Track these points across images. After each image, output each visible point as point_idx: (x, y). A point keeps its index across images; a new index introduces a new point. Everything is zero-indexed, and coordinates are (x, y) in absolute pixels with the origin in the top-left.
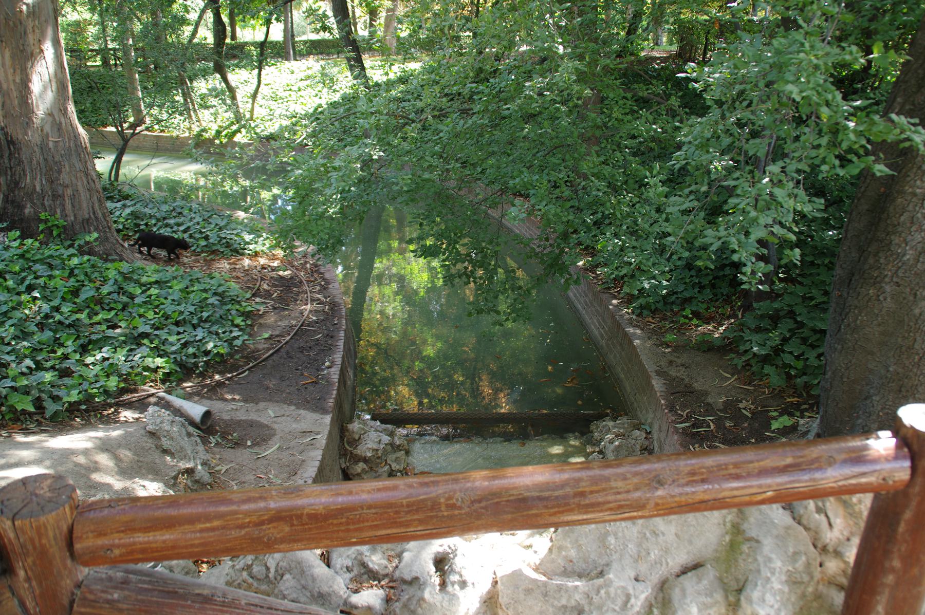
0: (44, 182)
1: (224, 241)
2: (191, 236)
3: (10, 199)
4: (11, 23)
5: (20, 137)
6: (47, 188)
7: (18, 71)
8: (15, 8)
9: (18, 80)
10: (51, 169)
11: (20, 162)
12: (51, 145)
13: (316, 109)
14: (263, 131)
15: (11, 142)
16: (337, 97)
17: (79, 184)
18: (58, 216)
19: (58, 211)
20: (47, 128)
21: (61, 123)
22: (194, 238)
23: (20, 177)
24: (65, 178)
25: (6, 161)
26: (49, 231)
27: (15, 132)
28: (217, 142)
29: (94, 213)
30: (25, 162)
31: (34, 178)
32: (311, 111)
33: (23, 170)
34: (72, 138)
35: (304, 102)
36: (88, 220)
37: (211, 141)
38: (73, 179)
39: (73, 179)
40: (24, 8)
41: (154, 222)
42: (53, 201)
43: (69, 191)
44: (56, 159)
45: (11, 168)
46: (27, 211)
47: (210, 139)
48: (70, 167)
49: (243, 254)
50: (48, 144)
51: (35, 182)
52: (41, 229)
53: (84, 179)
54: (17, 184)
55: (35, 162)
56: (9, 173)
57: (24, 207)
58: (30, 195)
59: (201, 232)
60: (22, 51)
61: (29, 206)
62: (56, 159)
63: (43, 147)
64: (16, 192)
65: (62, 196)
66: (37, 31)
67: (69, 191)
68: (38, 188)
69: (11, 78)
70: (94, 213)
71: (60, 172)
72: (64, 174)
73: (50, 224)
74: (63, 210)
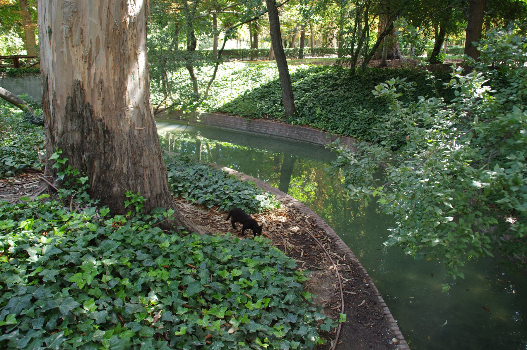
0: (130, 165)
1: (245, 201)
2: (217, 197)
3: (102, 179)
4: (117, 32)
5: (114, 127)
6: (131, 170)
7: (118, 72)
8: (121, 20)
9: (116, 80)
10: (135, 153)
11: (113, 148)
12: (136, 133)
13: (246, 93)
14: (214, 106)
15: (106, 131)
16: (258, 86)
17: (155, 165)
18: (139, 194)
19: (139, 189)
20: (135, 119)
21: (144, 114)
22: (221, 198)
23: (111, 161)
24: (145, 160)
25: (102, 148)
26: (133, 207)
27: (112, 125)
28: (184, 112)
29: (164, 189)
30: (117, 148)
31: (122, 162)
32: (243, 94)
33: (115, 155)
34: (151, 127)
35: (237, 88)
36: (160, 195)
37: (180, 112)
38: (151, 161)
39: (151, 161)
40: (128, 19)
41: (188, 184)
42: (135, 180)
43: (148, 172)
44: (139, 145)
45: (105, 153)
46: (115, 189)
47: (178, 110)
48: (149, 151)
49: (257, 212)
50: (134, 132)
51: (122, 164)
52: (126, 206)
53: (158, 160)
54: (108, 166)
55: (124, 148)
56: (103, 157)
57: (113, 186)
58: (118, 176)
59: (225, 194)
60: (122, 55)
61: (116, 185)
62: (139, 145)
63: (131, 135)
64: (107, 174)
65: (142, 176)
66: (134, 38)
67: (148, 172)
68: (125, 170)
69: (111, 77)
70: (164, 189)
71: (141, 155)
72: (144, 156)
73: (133, 201)
74: (143, 188)
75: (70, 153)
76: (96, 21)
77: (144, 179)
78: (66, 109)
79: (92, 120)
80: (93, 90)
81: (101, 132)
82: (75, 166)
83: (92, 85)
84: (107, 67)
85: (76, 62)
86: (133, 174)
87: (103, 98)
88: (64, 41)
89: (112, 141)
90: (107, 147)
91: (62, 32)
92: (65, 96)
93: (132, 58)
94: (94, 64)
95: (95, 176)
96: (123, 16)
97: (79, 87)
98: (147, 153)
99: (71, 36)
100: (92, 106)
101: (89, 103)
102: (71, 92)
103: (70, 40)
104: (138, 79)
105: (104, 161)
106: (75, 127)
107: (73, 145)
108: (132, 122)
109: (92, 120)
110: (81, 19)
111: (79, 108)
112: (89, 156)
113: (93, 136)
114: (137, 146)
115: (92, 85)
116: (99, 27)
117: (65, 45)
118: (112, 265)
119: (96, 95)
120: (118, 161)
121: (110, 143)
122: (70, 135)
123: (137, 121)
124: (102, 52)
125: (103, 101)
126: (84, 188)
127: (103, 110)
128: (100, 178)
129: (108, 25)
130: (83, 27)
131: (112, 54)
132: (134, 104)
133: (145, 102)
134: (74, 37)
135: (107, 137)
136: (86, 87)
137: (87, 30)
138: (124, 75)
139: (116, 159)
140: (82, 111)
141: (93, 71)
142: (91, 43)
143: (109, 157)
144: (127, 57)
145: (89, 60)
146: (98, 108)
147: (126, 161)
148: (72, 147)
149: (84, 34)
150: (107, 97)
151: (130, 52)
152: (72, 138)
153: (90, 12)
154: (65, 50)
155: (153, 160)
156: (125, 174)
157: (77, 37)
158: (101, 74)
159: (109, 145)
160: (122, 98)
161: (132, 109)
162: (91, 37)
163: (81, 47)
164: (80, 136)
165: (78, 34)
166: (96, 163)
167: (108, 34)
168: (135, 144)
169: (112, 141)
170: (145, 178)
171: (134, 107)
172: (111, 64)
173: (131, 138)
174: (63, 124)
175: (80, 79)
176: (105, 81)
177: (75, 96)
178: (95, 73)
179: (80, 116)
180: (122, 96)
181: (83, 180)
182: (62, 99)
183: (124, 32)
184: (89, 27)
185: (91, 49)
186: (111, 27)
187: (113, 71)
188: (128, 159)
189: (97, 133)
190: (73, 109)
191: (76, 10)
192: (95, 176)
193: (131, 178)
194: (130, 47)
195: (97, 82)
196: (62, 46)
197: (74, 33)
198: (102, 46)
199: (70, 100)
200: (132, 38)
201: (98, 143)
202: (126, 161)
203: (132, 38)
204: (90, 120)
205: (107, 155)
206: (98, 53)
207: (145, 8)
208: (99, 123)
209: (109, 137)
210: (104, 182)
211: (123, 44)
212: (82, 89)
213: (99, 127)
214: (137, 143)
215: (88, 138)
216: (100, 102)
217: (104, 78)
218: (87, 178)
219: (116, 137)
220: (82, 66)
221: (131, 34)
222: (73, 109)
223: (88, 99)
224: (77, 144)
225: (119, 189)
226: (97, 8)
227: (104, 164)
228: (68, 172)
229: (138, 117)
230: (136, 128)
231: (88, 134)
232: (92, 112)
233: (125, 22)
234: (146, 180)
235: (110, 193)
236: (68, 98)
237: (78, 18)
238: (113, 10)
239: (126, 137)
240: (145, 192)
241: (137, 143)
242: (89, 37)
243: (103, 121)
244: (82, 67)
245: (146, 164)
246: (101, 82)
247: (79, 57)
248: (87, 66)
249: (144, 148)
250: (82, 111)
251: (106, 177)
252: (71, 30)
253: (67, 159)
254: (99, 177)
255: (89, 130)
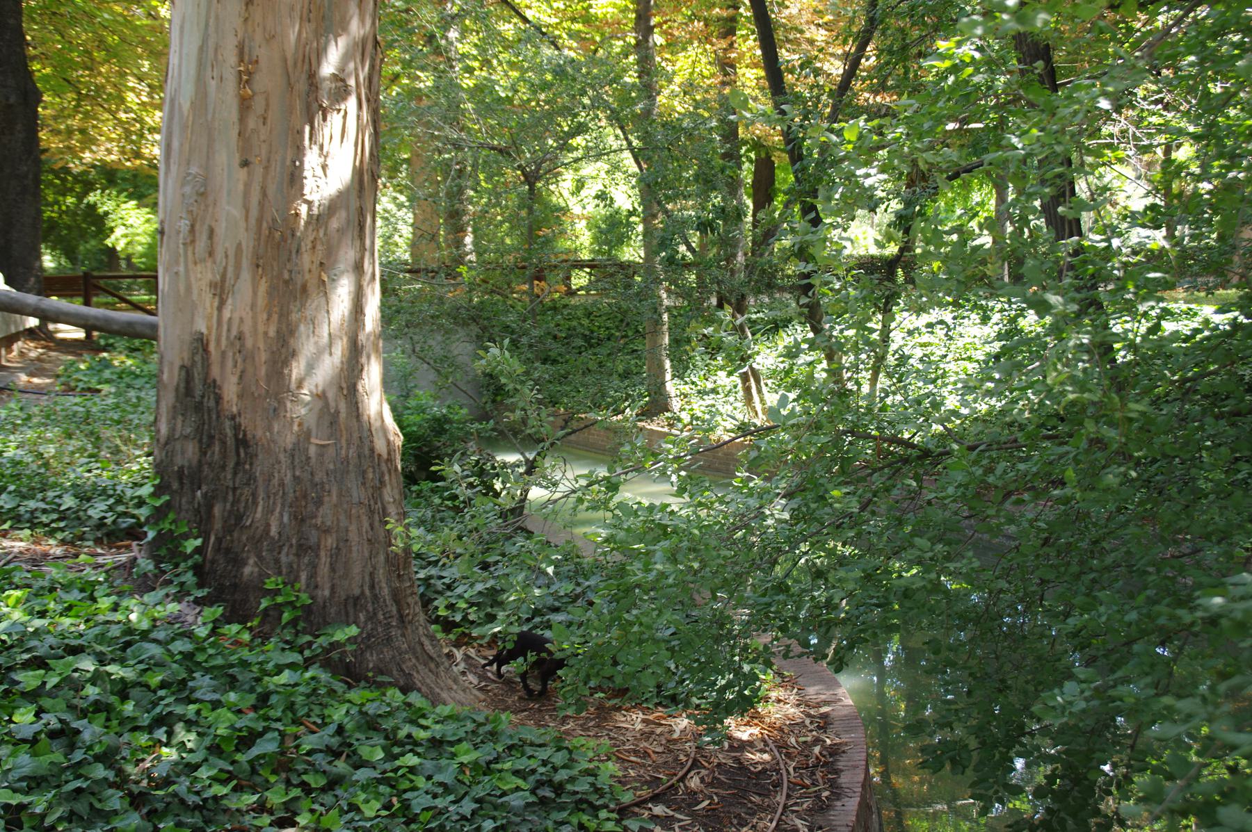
3: (224, 545)
5: (259, 433)
9: (272, 333)
11: (251, 479)
12: (312, 451)
15: (242, 442)
17: (353, 528)
19: (303, 576)
20: (312, 422)
21: (337, 412)
25: (229, 476)
27: (255, 427)
31: (269, 511)
38: (342, 517)
42: (298, 555)
43: (330, 541)
44: (317, 479)
45: (235, 489)
46: (247, 570)
54: (239, 518)
55: (275, 481)
56: (230, 498)
60: (286, 282)
61: (251, 561)
62: (317, 479)
64: (236, 534)
65: (316, 549)
67: (330, 541)
68: (274, 531)
69: (261, 329)
71: (319, 503)
72: (326, 506)
73: (280, 600)
74: (312, 576)
75: (175, 486)
76: (237, 213)
77: (318, 556)
78: (177, 390)
79: (218, 417)
80: (224, 353)
81: (230, 442)
82: (183, 514)
83: (224, 342)
84: (253, 306)
85: (200, 295)
86: (294, 541)
87: (242, 372)
88: (181, 251)
89: (251, 464)
90: (240, 475)
91: (178, 232)
92: (178, 363)
93: (312, 287)
94: (230, 301)
95: (212, 539)
96: (293, 202)
97: (201, 344)
98: (335, 498)
99: (193, 242)
100: (220, 388)
101: (214, 381)
102: (186, 355)
103: (190, 249)
104: (326, 334)
105: (232, 505)
106: (189, 430)
107: (181, 468)
108: (306, 425)
109: (218, 417)
110: (210, 209)
111: (198, 390)
112: (206, 493)
113: (217, 449)
114: (311, 481)
115: (224, 342)
116: (242, 224)
117: (182, 260)
118: (122, 679)
119: (230, 363)
120: (260, 509)
121: (247, 467)
122: (178, 446)
123: (318, 425)
124: (246, 275)
125: (241, 377)
126: (190, 563)
127: (240, 396)
128: (220, 543)
129: (260, 221)
130: (213, 224)
131: (264, 279)
132: (313, 388)
133: (344, 385)
134: (197, 243)
135: (242, 455)
136: (212, 347)
137: (221, 230)
138: (288, 325)
139: (255, 503)
140: (203, 397)
141: (227, 314)
142: (227, 256)
143: (243, 498)
144: (299, 286)
145: (221, 290)
146: (230, 391)
147: (278, 510)
148: (180, 474)
149: (216, 239)
150: (250, 370)
151: (307, 276)
152: (183, 453)
153: (229, 194)
154: (182, 269)
155: (350, 517)
156: (273, 538)
157: (203, 245)
158: (241, 320)
159: (245, 471)
160: (282, 373)
161: (308, 398)
162: (227, 245)
163: (209, 264)
164: (197, 450)
165: (204, 237)
166: (217, 510)
167: (259, 239)
168: (306, 476)
169: (251, 464)
170: (322, 553)
171: (312, 394)
172: (261, 301)
173: (297, 461)
174: (169, 422)
175: (204, 330)
176: (247, 335)
177: (194, 363)
178: (230, 319)
179: (199, 407)
180: (282, 368)
181: (192, 544)
182: (171, 371)
183: (293, 235)
184: (224, 225)
185: (225, 268)
186: (265, 225)
187: (265, 316)
188: (283, 505)
189: (224, 443)
190: (189, 391)
191: (202, 190)
192: (212, 539)
193: (285, 549)
194: (307, 266)
195: (232, 337)
196: (177, 263)
197: (197, 234)
198: (245, 263)
199: (183, 373)
200: (314, 247)
201: (223, 467)
202: (278, 510)
203: (314, 247)
204: (214, 417)
205: (238, 492)
206: (237, 277)
207: (361, 181)
208: (228, 423)
209: (246, 454)
210: (228, 551)
211: (289, 260)
212: (206, 350)
213: (228, 430)
214: (312, 474)
215: (209, 454)
216: (234, 379)
217: (247, 329)
218: (199, 542)
219: (260, 457)
220: (208, 302)
221: (311, 238)
222: (189, 391)
223: (215, 372)
224: (190, 467)
225: (256, 570)
226: (241, 187)
227: (230, 512)
228: (166, 526)
229: (320, 418)
230: (313, 440)
231: (209, 446)
232: (219, 399)
233: (297, 215)
234: (323, 559)
235: (235, 577)
236: (182, 367)
237: (207, 206)
238: (272, 190)
239: (282, 457)
240: (316, 587)
241: (312, 474)
242: (224, 243)
243: (237, 420)
244: (208, 305)
245: (329, 523)
246: (240, 337)
247: (204, 284)
248: (216, 304)
249: (327, 487)
250: (203, 397)
251: (232, 541)
252: (192, 229)
253: (168, 498)
254: (219, 540)
255: (211, 437)
